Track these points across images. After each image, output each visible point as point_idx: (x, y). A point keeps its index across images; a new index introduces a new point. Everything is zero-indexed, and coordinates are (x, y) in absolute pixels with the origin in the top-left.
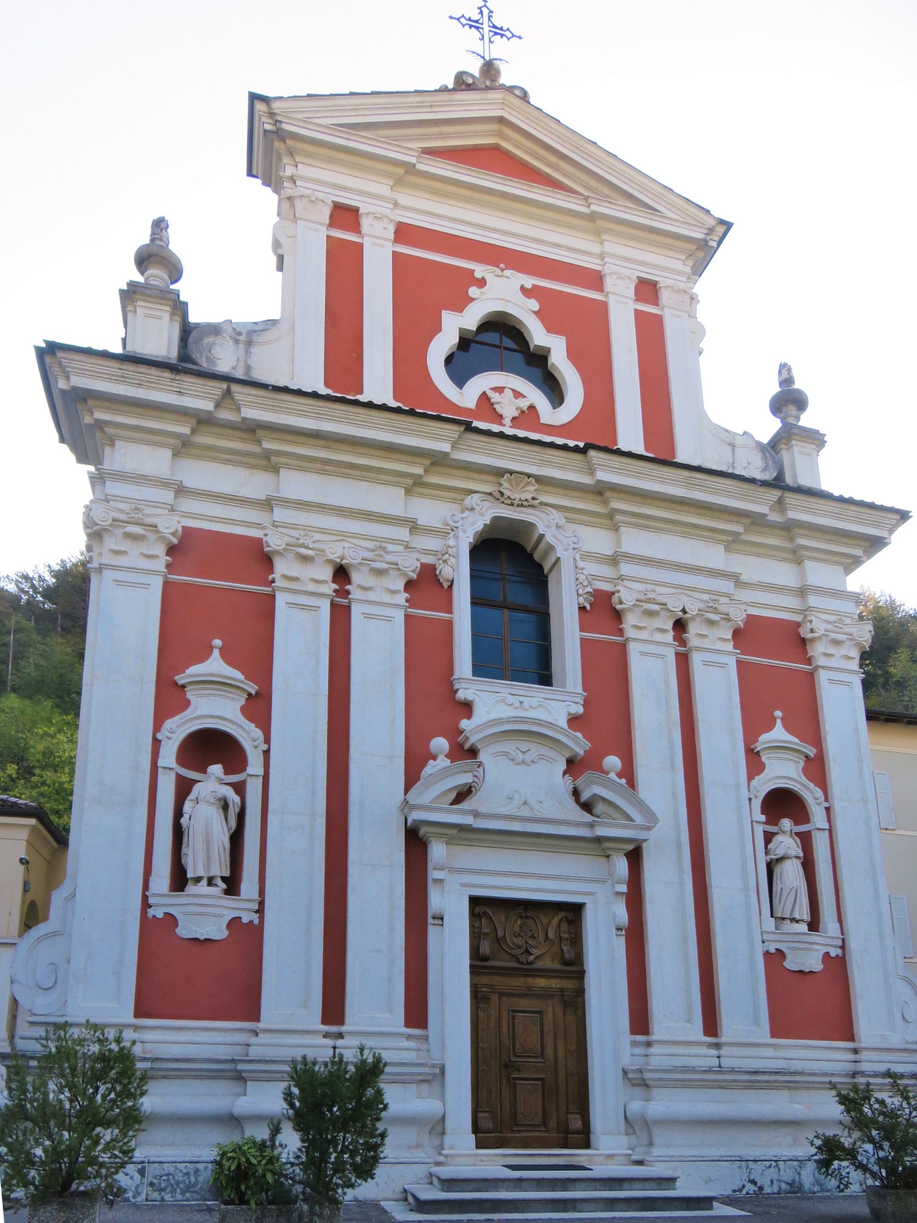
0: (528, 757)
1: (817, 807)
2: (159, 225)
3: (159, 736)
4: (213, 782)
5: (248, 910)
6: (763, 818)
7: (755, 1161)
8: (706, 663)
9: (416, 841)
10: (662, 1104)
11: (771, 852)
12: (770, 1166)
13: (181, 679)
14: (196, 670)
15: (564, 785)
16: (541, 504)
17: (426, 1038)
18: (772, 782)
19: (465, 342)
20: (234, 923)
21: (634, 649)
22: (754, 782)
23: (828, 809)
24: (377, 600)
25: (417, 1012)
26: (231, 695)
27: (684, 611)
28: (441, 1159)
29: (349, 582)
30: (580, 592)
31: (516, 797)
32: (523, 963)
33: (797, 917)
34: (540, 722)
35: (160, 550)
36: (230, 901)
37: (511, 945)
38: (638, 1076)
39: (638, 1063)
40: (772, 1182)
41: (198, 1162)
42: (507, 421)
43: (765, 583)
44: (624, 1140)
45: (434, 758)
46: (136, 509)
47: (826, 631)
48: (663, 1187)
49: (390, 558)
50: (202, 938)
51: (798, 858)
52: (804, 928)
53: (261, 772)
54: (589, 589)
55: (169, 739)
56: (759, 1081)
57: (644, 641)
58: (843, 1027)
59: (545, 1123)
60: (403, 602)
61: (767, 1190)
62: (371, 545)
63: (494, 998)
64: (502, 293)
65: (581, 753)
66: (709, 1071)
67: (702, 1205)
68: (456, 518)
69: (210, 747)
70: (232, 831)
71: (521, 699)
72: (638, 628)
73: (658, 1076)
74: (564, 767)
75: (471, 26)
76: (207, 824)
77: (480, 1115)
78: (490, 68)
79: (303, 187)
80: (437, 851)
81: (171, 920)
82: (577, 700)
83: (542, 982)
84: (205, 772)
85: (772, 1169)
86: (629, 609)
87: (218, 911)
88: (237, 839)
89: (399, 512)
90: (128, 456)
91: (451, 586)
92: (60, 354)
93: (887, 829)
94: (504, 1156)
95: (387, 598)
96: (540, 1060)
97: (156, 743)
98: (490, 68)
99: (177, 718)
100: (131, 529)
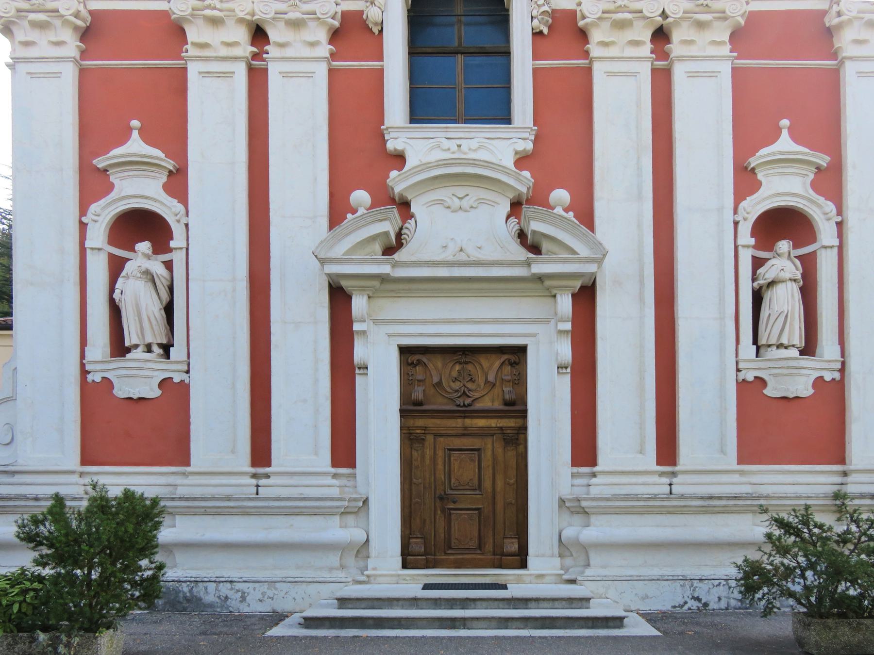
0: (465, 203)
1: (826, 223)
3: (84, 219)
5: (179, 371)
6: (752, 241)
7: (700, 580)
9: (339, 296)
10: (597, 530)
11: (761, 277)
12: (719, 584)
13: (753, 162)
17: (354, 476)
18: (768, 202)
21: (599, 71)
22: (743, 204)
23: (840, 225)
24: (298, 55)
25: (344, 452)
28: (363, 578)
32: (459, 406)
37: (448, 390)
38: (576, 504)
39: (579, 492)
40: (720, 599)
47: (858, 12)
48: (573, 606)
50: (135, 397)
51: (795, 280)
53: (836, 242)
54: (546, 8)
56: (714, 506)
57: (612, 59)
59: (480, 546)
60: (648, 54)
61: (713, 605)
63: (430, 439)
65: (524, 190)
67: (611, 624)
69: (141, 227)
71: (459, 142)
73: (594, 504)
74: (507, 208)
76: (139, 300)
80: (359, 304)
81: (107, 383)
82: (526, 135)
83: (481, 423)
85: (721, 587)
86: (594, 24)
88: (169, 309)
91: (381, 31)
94: (428, 576)
96: (477, 492)
97: (83, 226)
99: (103, 202)
100: (32, 16)
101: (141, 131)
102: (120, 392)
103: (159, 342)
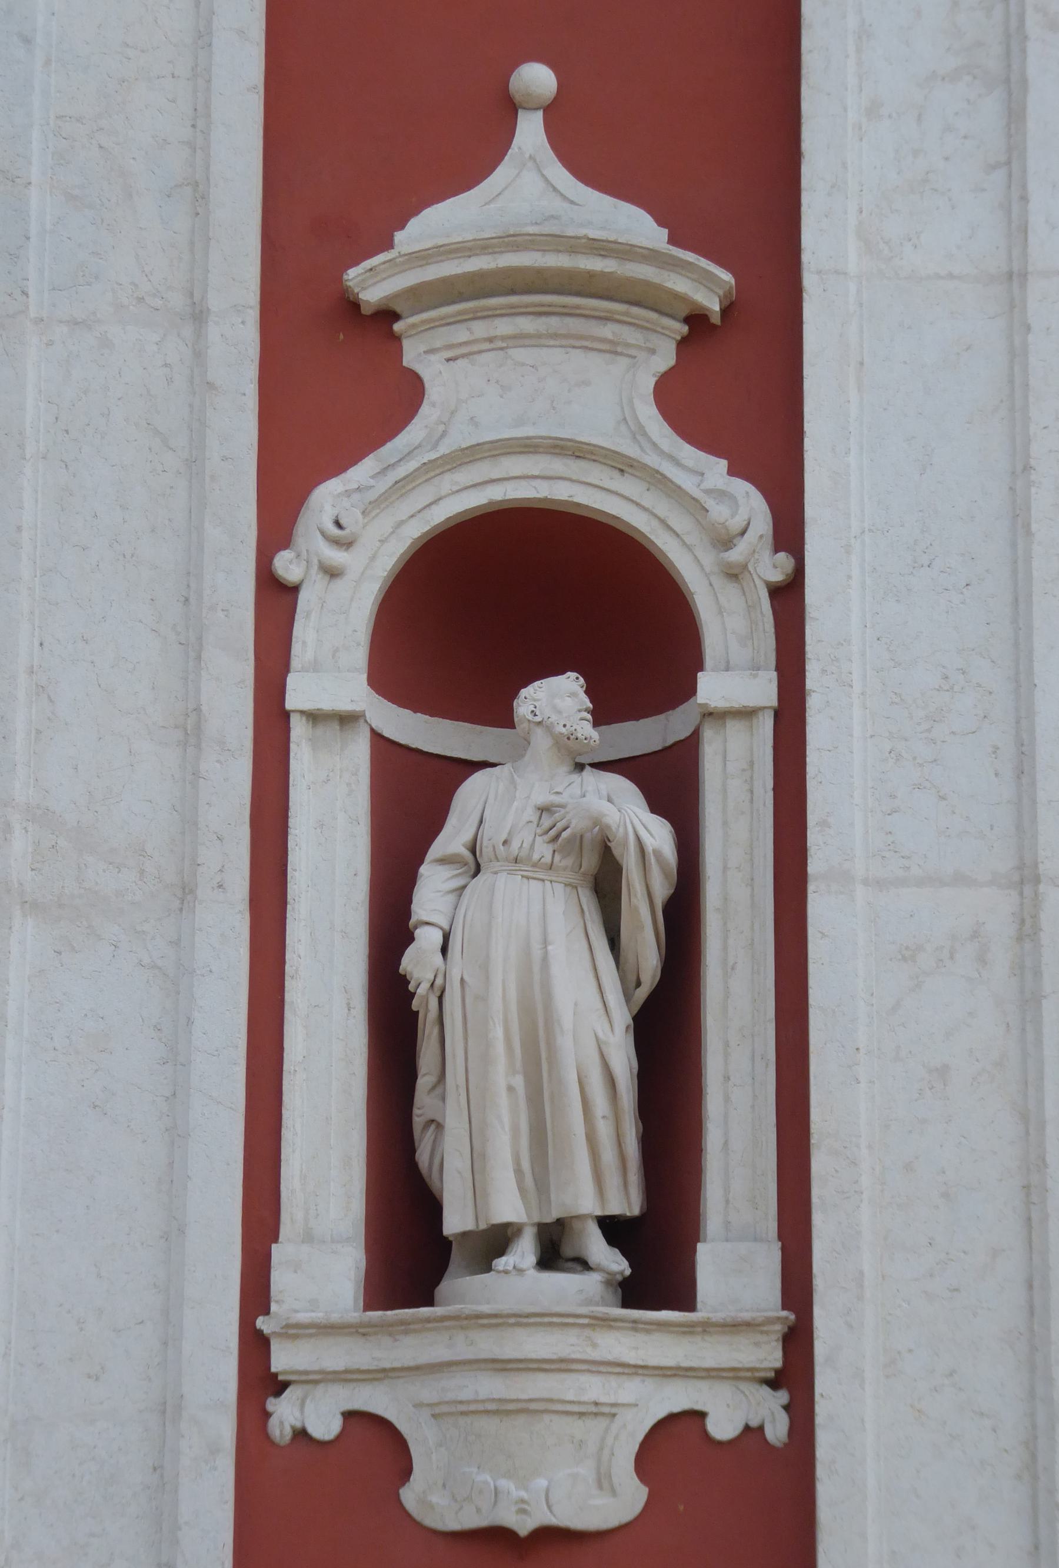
1: (731, 595)
4: (546, 763)
13: (372, 282)
14: (443, 227)
20: (673, 1443)
26: (607, 331)
36: (650, 1340)
50: (524, 1526)
53: (762, 690)
55: (332, 573)
70: (642, 994)
76: (530, 971)
81: (378, 1446)
84: (502, 716)
87: (593, 1388)
97: (276, 599)
101: (556, 116)
102: (436, 1499)
103: (599, 1213)
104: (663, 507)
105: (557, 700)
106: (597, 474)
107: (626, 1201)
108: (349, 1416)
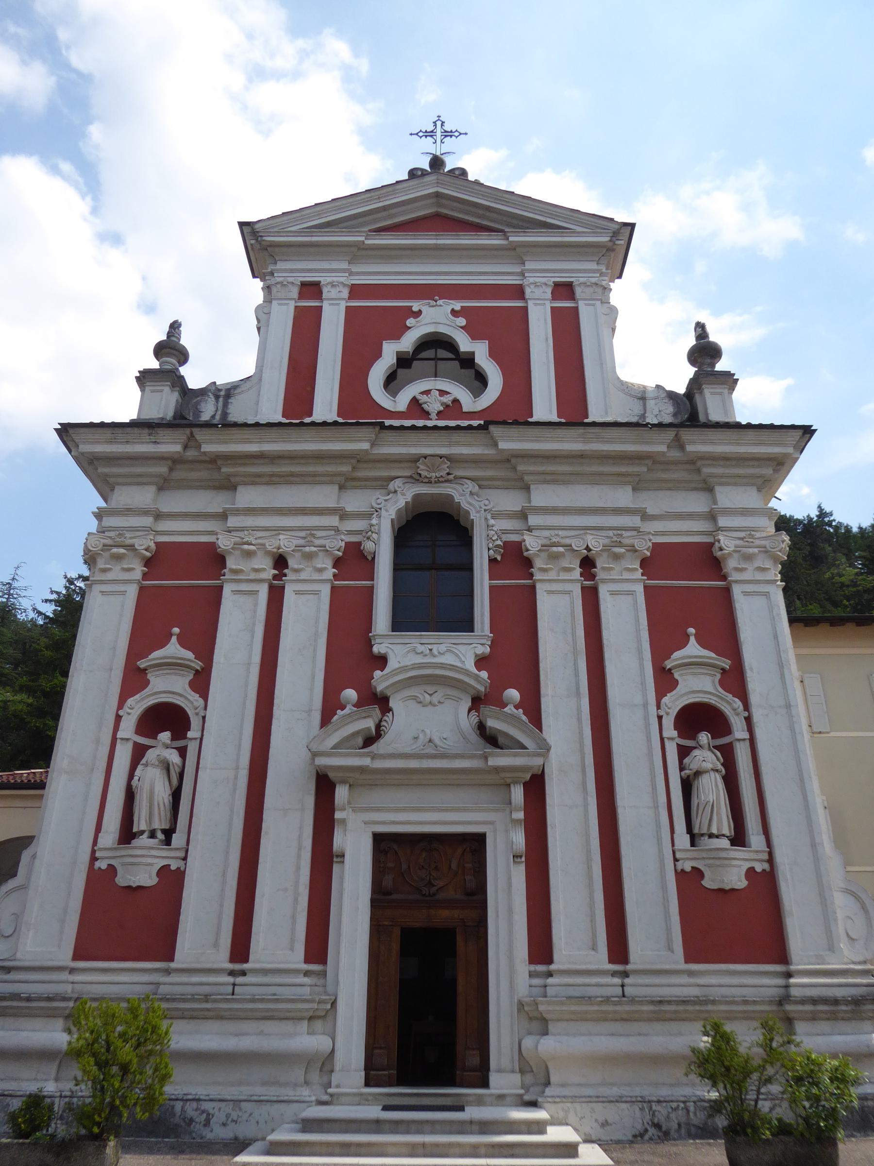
0: (435, 699)
2: (175, 327)
3: (121, 713)
4: (163, 747)
6: (675, 734)
8: (613, 593)
9: (325, 786)
13: (669, 664)
14: (678, 655)
15: (466, 721)
16: (456, 478)
17: (324, 974)
18: (685, 698)
19: (404, 361)
20: (751, 872)
25: (317, 947)
27: (588, 549)
28: (325, 1098)
29: (287, 567)
30: (491, 545)
31: (421, 736)
33: (714, 831)
34: (442, 666)
35: (328, 564)
36: (738, 853)
40: (679, 1125)
41: (672, 1101)
42: (433, 415)
43: (674, 515)
44: (517, 1078)
45: (343, 708)
46: (120, 534)
49: (318, 542)
50: (134, 885)
52: (725, 843)
53: (746, 735)
55: (129, 714)
57: (550, 581)
58: (776, 950)
62: (303, 534)
64: (435, 318)
65: (482, 689)
66: (607, 1000)
68: (379, 501)
70: (173, 789)
71: (430, 647)
72: (737, 569)
75: (426, 136)
76: (154, 785)
77: (376, 1051)
78: (437, 162)
79: (279, 277)
80: (341, 793)
81: (112, 869)
84: (155, 737)
86: (730, 554)
87: (149, 860)
88: (176, 795)
89: (332, 504)
90: (125, 496)
91: (374, 558)
92: (71, 431)
93: (820, 733)
95: (626, 575)
97: (118, 718)
98: (437, 162)
99: (137, 697)
101: (179, 637)
104: (187, 702)
105: (165, 736)
106: (182, 699)
107: (166, 826)
108: (693, 868)
